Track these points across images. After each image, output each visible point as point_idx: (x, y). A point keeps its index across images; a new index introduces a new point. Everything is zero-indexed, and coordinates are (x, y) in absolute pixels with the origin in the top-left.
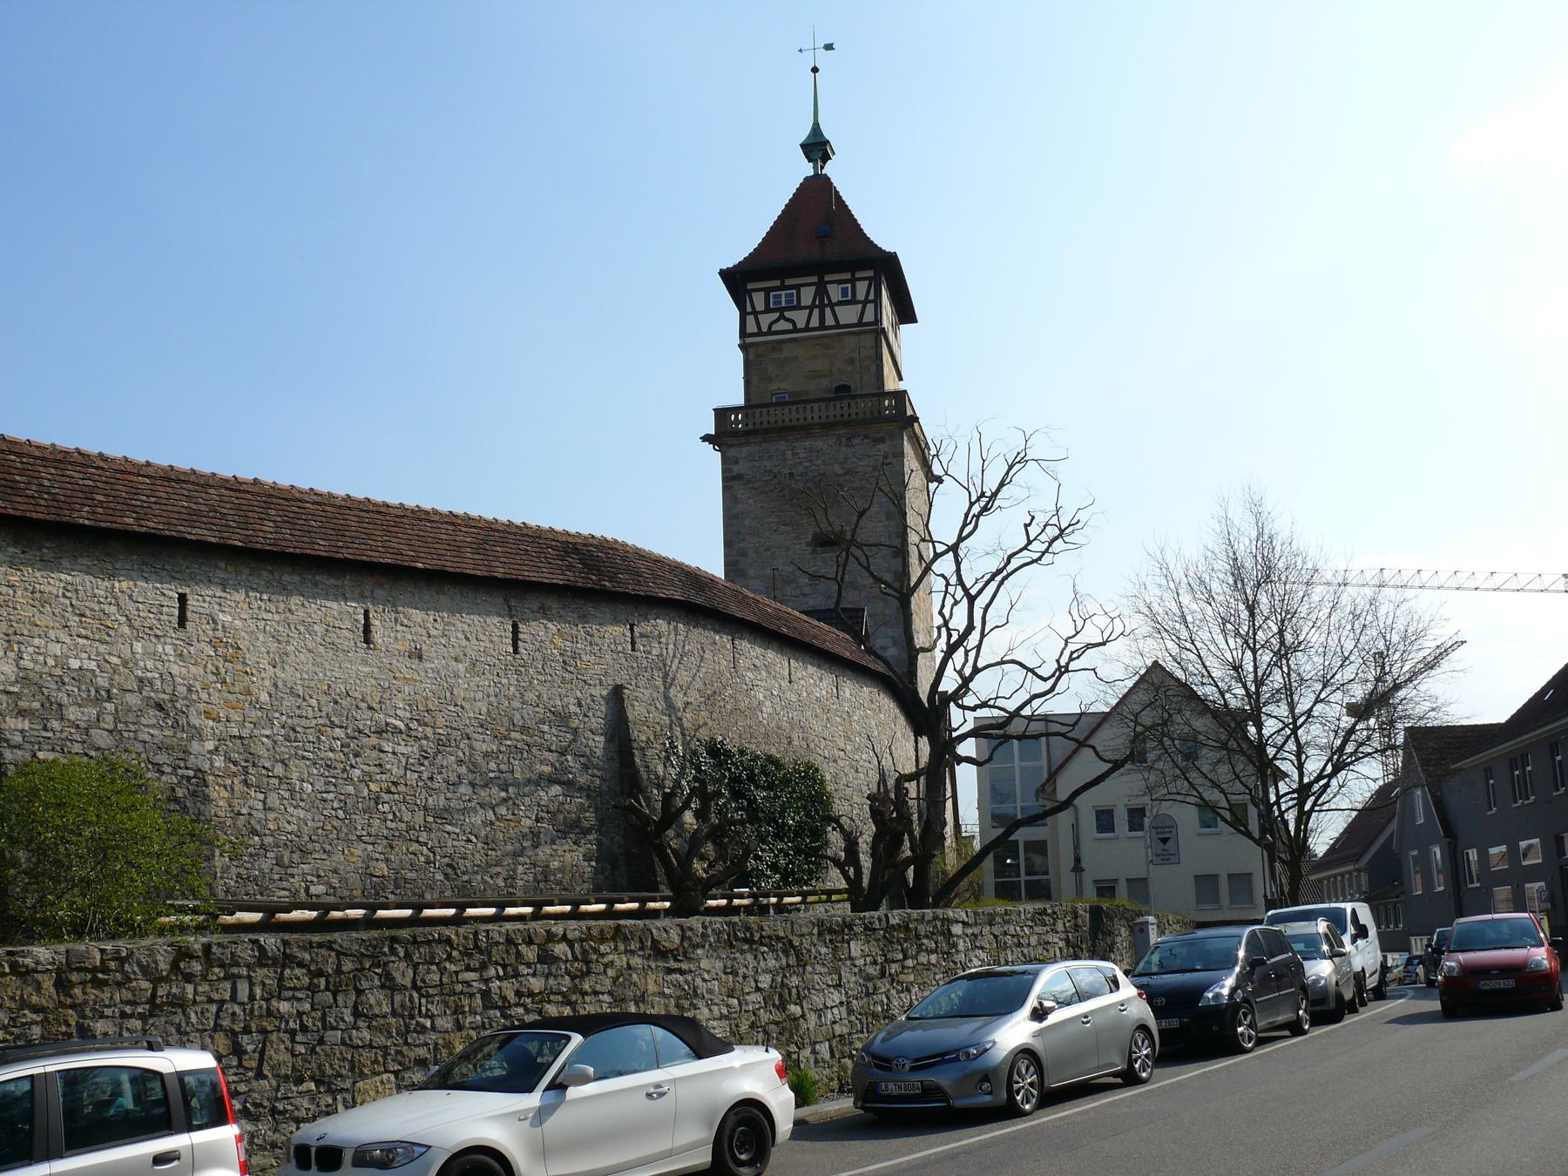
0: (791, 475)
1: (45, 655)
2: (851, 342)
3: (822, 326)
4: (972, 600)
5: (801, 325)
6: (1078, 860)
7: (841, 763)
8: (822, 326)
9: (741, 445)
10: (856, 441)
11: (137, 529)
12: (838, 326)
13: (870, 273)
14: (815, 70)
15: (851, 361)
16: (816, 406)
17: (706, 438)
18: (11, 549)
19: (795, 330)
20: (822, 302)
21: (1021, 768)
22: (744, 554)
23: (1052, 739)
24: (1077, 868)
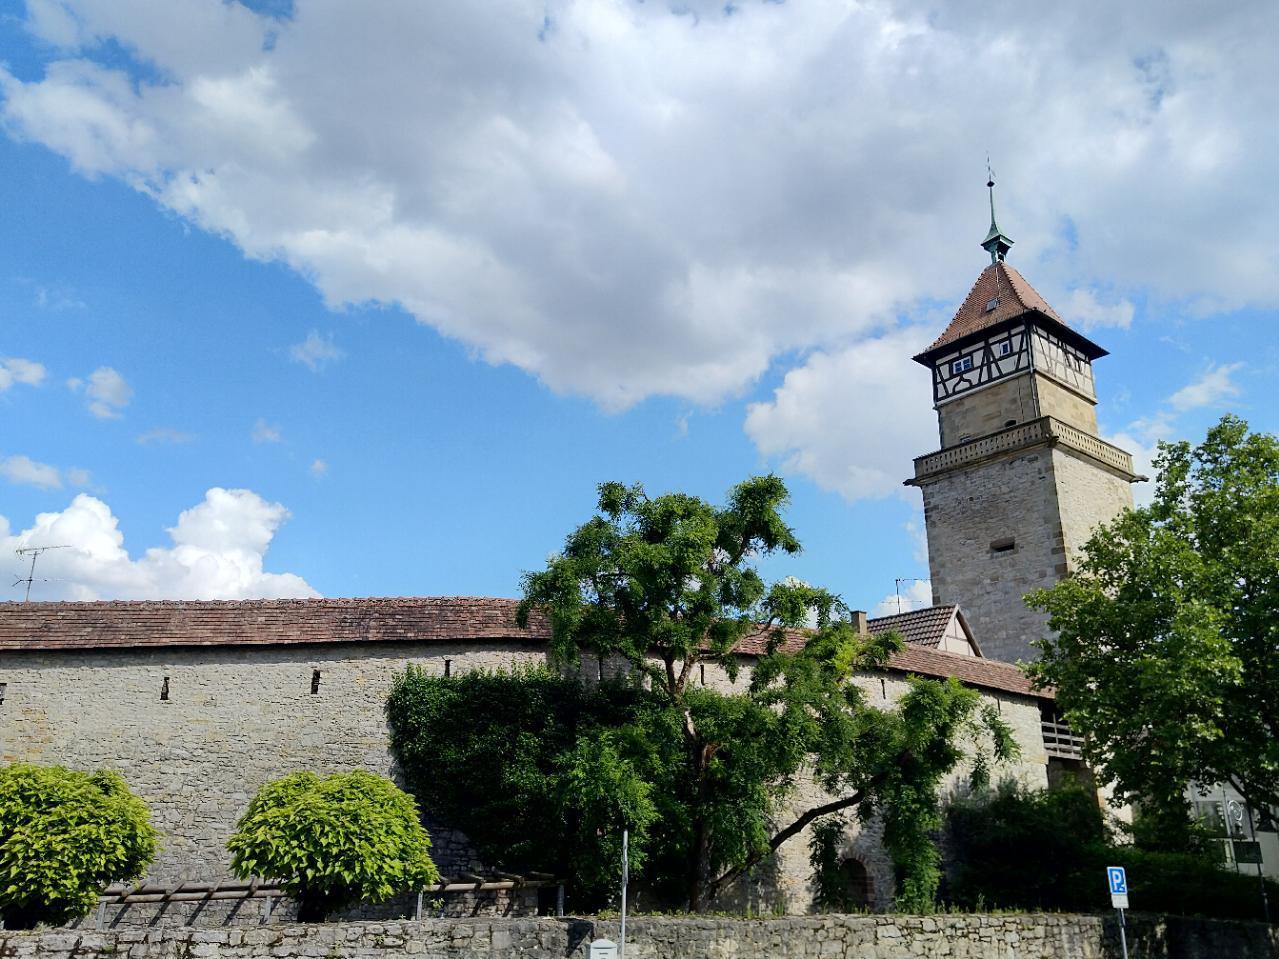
0: (971, 499)
5: (975, 382)
8: (991, 379)
12: (1002, 376)
16: (983, 442)
20: (989, 360)
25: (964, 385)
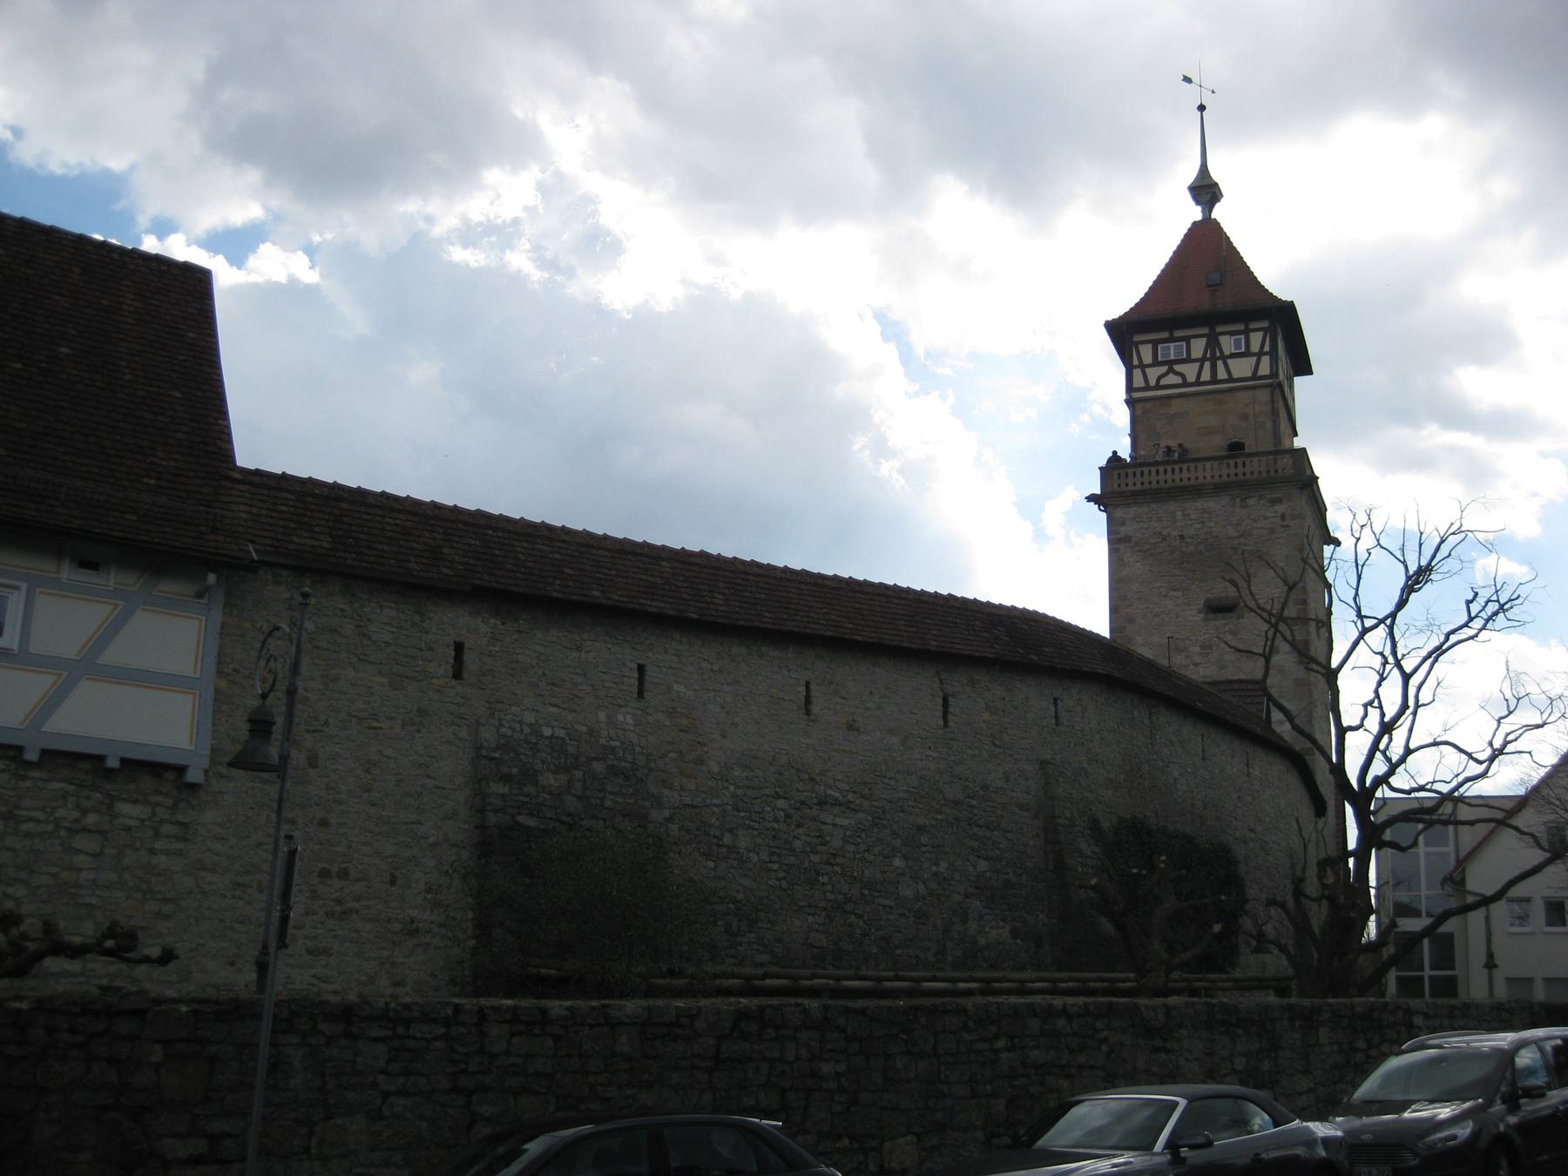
0: (1182, 537)
1: (520, 722)
2: (1244, 396)
3: (1214, 380)
4: (1406, 677)
5: (1191, 378)
6: (1490, 955)
7: (1251, 844)
8: (1214, 380)
9: (1128, 505)
10: (1251, 502)
11: (605, 602)
12: (1231, 379)
13: (1265, 324)
14: (1202, 108)
15: (1245, 417)
16: (1208, 464)
17: (1091, 498)
18: (493, 621)
19: (1185, 384)
20: (1214, 355)
21: (1427, 855)
22: (1131, 620)
23: (1461, 827)
24: (1491, 965)
25: (1172, 379)
